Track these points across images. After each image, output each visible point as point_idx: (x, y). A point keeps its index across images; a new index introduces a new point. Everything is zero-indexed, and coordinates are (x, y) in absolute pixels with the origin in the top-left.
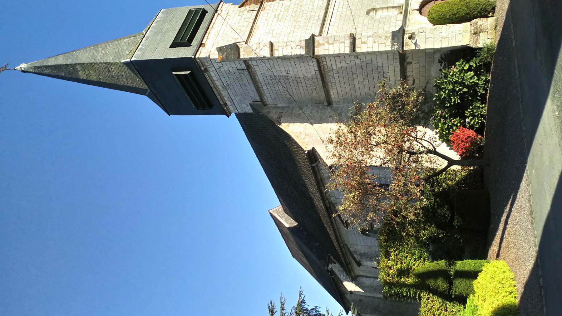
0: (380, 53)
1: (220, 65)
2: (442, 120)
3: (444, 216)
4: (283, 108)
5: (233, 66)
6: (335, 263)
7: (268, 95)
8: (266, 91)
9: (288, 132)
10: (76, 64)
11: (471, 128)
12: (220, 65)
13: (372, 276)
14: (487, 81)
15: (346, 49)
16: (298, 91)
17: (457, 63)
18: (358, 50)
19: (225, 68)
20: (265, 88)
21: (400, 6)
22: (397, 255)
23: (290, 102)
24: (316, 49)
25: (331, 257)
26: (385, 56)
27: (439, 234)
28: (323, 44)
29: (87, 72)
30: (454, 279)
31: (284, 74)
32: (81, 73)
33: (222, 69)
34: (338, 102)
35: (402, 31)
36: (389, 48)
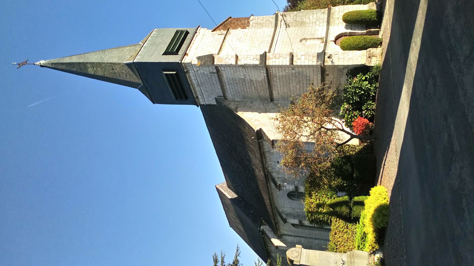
0: (309, 66)
1: (198, 69)
2: (347, 112)
3: (347, 170)
4: (239, 102)
5: (207, 70)
6: (265, 225)
7: (229, 92)
8: (228, 89)
9: (243, 118)
10: (87, 63)
11: (366, 117)
12: (198, 69)
13: (293, 234)
14: (376, 88)
15: (286, 62)
16: (251, 90)
17: (358, 76)
18: (295, 63)
19: (202, 71)
20: (227, 87)
21: (322, 38)
22: (316, 196)
23: (244, 97)
24: (267, 61)
25: (263, 221)
26: (311, 69)
27: (344, 184)
28: (272, 58)
29: (95, 69)
30: (353, 206)
31: (243, 77)
32: (90, 69)
33: (199, 72)
34: (278, 99)
35: (324, 53)
36: (315, 64)
